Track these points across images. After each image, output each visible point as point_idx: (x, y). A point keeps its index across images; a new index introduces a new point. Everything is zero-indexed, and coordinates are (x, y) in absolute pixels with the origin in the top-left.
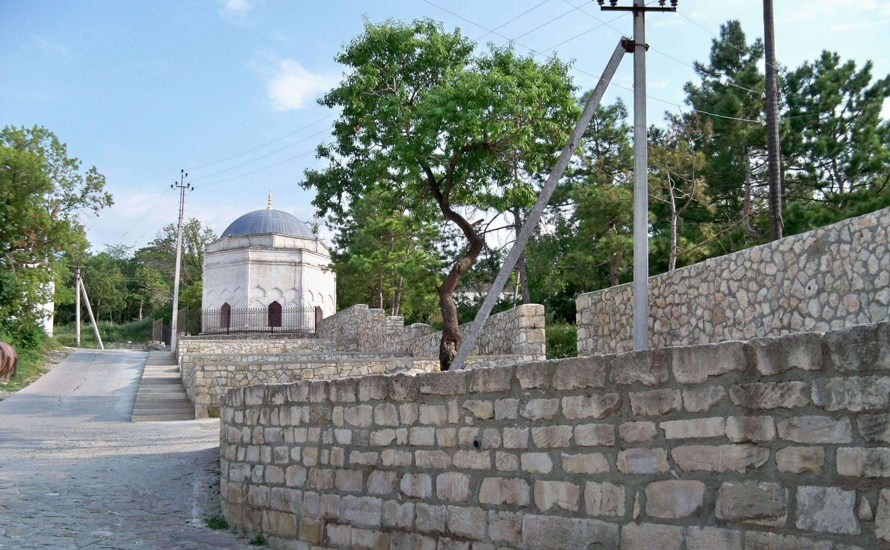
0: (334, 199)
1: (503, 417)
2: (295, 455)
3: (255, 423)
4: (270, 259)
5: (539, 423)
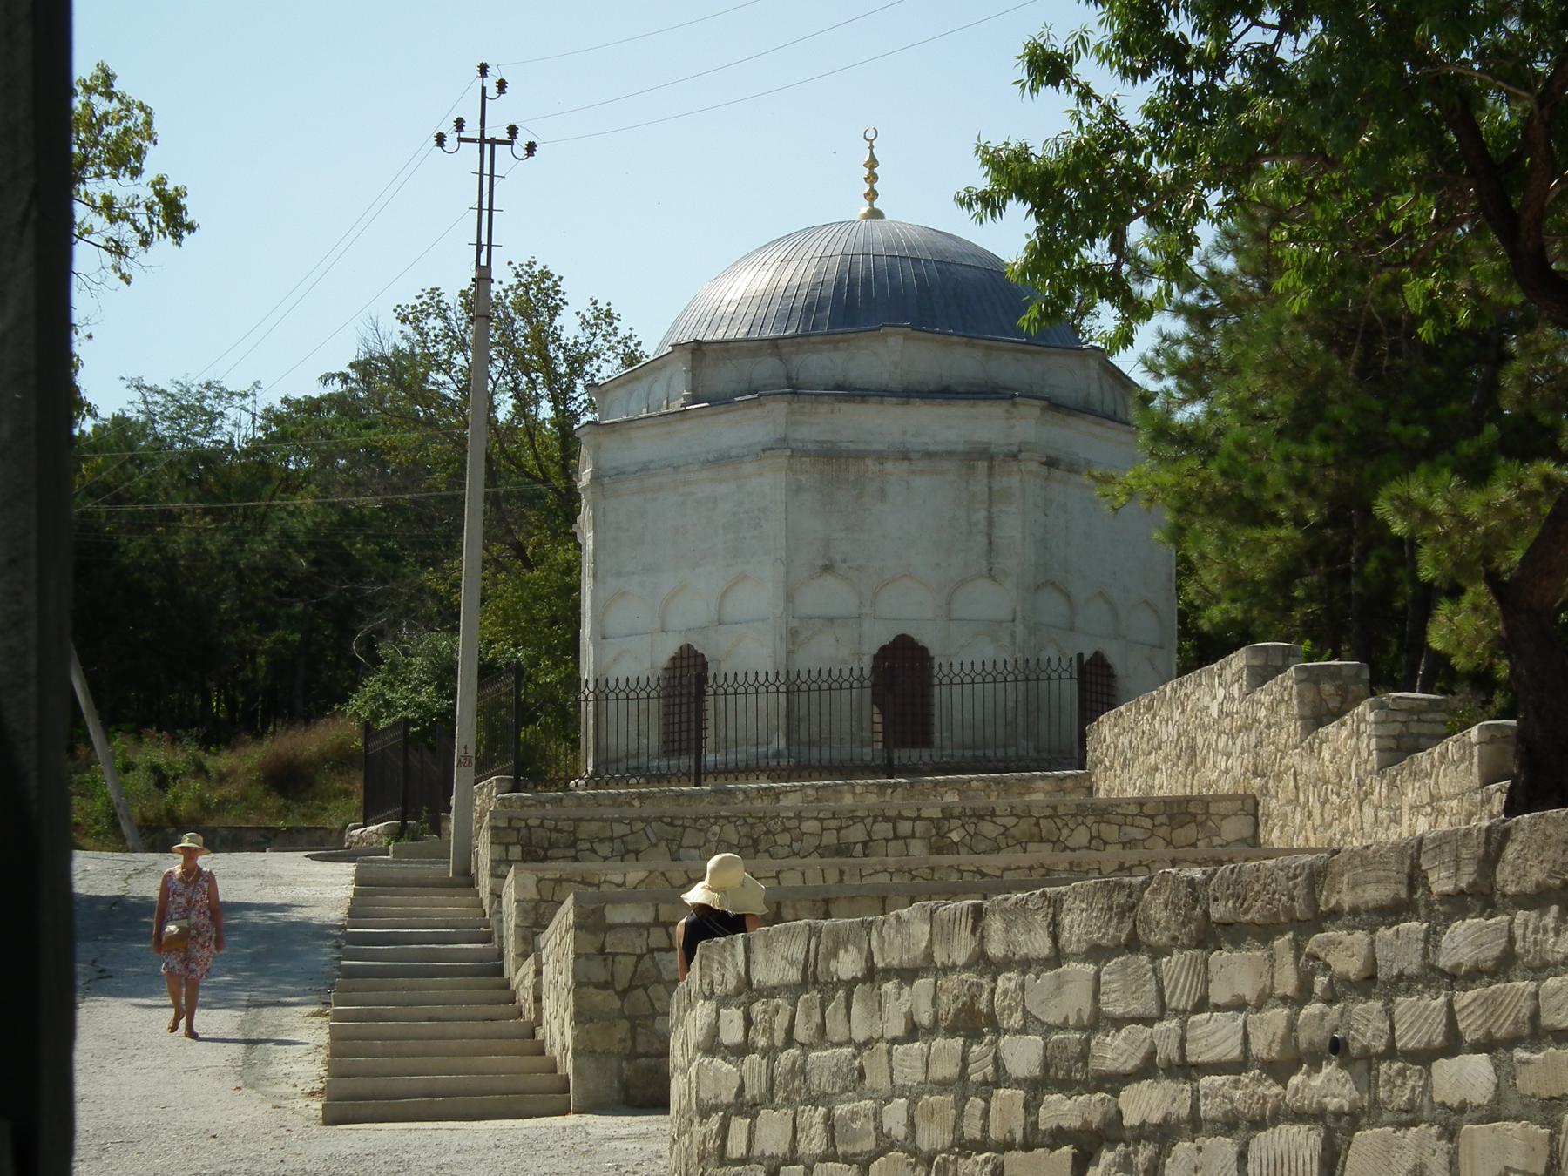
0: (1098, 253)
1: (1395, 972)
2: (895, 1116)
3: (779, 1041)
5: (1472, 975)
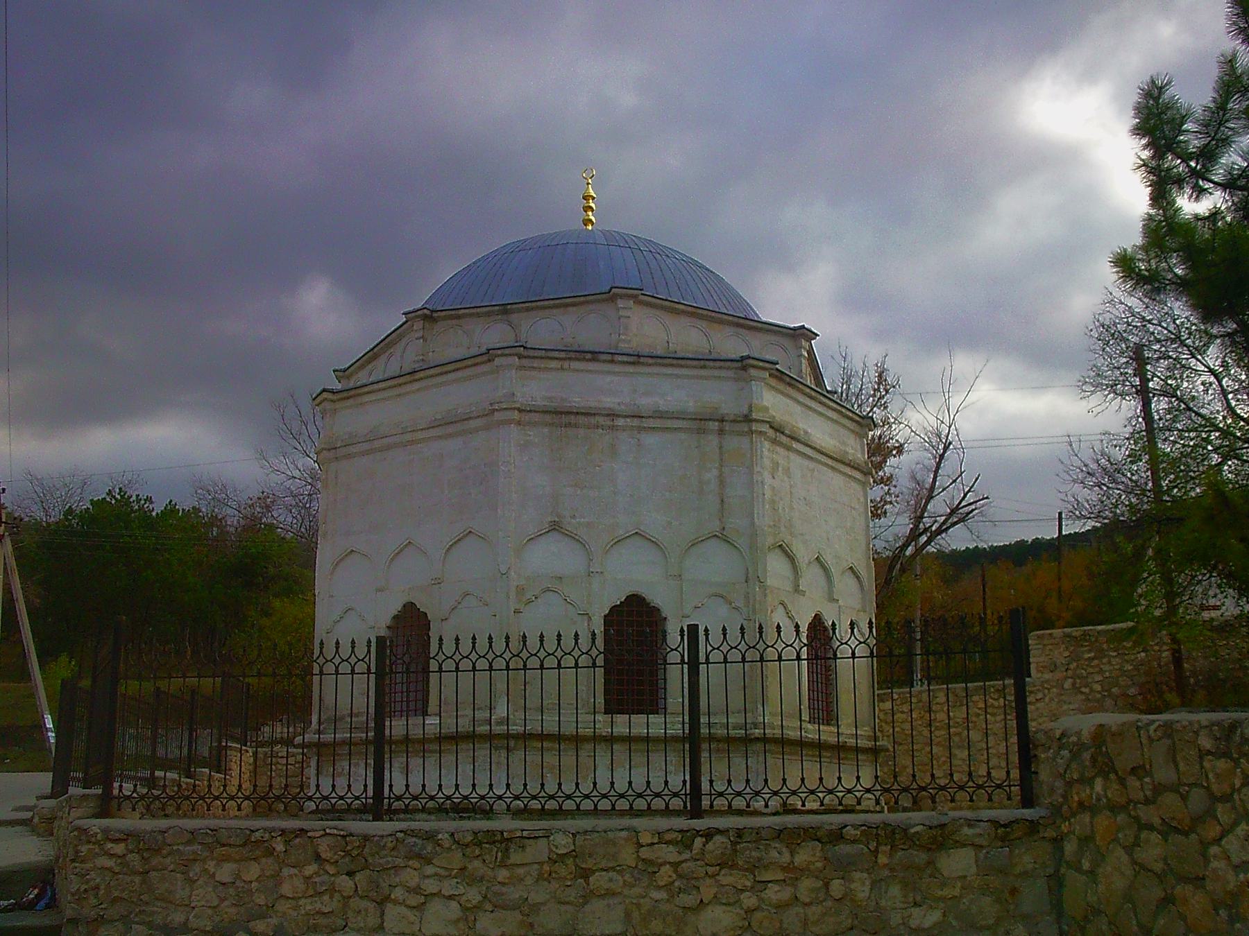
4: (609, 402)
